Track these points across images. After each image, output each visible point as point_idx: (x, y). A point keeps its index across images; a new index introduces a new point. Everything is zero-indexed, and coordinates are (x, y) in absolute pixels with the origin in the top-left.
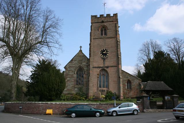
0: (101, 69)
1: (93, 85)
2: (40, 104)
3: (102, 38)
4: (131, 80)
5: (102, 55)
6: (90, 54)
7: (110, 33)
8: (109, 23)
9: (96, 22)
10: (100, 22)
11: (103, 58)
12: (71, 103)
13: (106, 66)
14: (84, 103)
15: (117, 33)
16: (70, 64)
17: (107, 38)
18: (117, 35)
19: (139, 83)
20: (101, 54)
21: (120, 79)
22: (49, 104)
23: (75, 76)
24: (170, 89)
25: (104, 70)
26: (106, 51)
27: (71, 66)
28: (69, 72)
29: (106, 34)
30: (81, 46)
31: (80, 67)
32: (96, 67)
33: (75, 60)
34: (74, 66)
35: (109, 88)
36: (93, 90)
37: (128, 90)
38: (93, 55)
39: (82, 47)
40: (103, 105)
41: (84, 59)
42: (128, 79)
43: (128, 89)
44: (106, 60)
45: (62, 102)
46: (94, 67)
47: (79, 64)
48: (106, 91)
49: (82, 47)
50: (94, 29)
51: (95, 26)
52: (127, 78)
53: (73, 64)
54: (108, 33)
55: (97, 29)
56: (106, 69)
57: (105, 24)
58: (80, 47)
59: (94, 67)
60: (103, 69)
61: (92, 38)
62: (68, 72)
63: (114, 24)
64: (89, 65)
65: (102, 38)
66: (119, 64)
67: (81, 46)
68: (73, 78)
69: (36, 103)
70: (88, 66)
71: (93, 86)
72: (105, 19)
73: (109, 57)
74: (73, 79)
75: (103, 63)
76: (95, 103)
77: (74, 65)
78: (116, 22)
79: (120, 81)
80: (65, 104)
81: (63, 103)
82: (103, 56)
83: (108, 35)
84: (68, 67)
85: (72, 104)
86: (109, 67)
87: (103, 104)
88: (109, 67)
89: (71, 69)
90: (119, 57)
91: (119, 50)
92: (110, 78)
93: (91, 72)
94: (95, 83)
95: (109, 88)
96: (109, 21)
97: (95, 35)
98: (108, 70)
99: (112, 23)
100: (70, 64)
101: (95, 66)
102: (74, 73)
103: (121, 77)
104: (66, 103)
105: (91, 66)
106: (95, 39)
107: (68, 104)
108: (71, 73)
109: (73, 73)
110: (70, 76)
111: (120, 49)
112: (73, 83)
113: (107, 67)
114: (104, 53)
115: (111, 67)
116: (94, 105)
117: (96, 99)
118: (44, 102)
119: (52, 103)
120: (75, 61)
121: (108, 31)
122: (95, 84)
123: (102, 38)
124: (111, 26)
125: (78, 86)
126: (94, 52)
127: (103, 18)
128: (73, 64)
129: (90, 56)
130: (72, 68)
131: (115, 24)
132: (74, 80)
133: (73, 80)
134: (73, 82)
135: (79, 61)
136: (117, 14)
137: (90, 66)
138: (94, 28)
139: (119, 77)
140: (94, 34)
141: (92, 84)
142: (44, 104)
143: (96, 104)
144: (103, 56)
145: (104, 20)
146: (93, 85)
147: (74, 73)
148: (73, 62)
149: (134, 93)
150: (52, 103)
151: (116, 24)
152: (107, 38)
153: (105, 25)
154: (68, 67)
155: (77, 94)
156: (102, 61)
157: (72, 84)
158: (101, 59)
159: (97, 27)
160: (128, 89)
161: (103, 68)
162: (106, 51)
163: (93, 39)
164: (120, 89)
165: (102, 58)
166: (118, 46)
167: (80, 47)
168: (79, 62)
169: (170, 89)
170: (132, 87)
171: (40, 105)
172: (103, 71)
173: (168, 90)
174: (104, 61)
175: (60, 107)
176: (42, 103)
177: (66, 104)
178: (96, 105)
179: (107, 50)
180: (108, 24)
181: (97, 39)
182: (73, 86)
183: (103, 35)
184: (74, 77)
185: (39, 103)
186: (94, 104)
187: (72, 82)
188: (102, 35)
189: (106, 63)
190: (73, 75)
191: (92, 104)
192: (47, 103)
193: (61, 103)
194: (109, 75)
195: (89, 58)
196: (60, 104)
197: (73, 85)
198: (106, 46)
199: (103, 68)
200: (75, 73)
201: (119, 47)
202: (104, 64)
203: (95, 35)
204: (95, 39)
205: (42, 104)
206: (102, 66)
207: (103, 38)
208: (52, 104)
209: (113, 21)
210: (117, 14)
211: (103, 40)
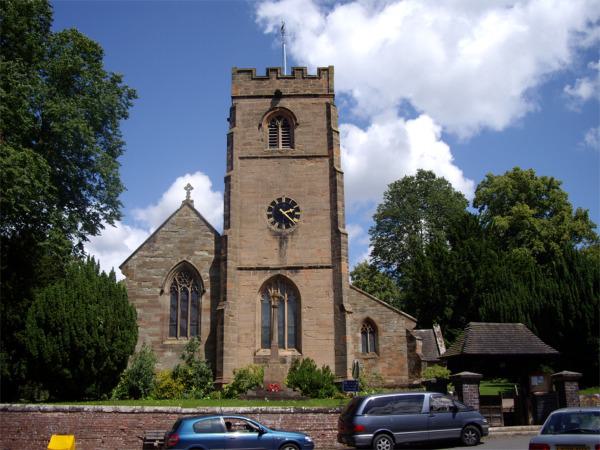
0: (269, 275)
1: (239, 339)
2: (48, 415)
3: (274, 157)
4: (376, 319)
5: (273, 223)
6: (227, 217)
7: (307, 138)
8: (303, 100)
9: (252, 94)
10: (266, 93)
11: (280, 234)
12: (255, 408)
13: (290, 263)
14: (232, 409)
15: (332, 138)
16: (146, 253)
17: (294, 157)
18: (332, 148)
19: (407, 331)
20: (269, 216)
21: (344, 316)
22: (87, 412)
23: (166, 300)
24: (549, 350)
25: (281, 286)
26: (291, 210)
27: (147, 260)
28: (140, 284)
29: (289, 141)
30: (189, 185)
31: (185, 266)
32: (251, 269)
33: (166, 240)
34: (161, 263)
35: (300, 351)
36: (241, 355)
37: (366, 359)
38: (241, 221)
39: (192, 188)
40: (310, 415)
41: (200, 234)
42: (365, 315)
43: (368, 356)
44: (290, 243)
45: (143, 405)
46: (240, 269)
47: (182, 253)
48: (289, 360)
49: (192, 188)
50: (243, 121)
51: (248, 109)
52: (363, 311)
53: (156, 253)
54: (298, 138)
55: (256, 123)
56: (288, 274)
57: (285, 103)
58: (186, 188)
59: (240, 269)
60: (279, 276)
61: (237, 153)
62: (136, 284)
63: (321, 104)
64: (225, 260)
65: (275, 155)
66: (340, 259)
67: (189, 185)
68: (159, 311)
69: (29, 411)
70: (219, 264)
71: (238, 342)
72: (286, 86)
73: (299, 231)
74: (156, 315)
75: (276, 254)
76: (280, 409)
77: (161, 259)
78: (328, 100)
79: (344, 321)
80: (156, 412)
81: (147, 409)
82: (277, 224)
83: (296, 145)
84: (139, 266)
85: (184, 410)
86: (302, 268)
87: (308, 412)
88: (302, 268)
89: (149, 274)
90: (341, 230)
91: (339, 204)
92: (303, 310)
93: (230, 287)
94: (248, 331)
95: (303, 349)
96: (302, 92)
97: (250, 144)
98: (299, 279)
99: (314, 100)
100: (146, 253)
101: (245, 264)
102: (162, 292)
103: (347, 309)
104: (160, 408)
105: (229, 263)
106: (248, 158)
107: (167, 413)
108: (146, 291)
109: (159, 290)
110: (146, 301)
111: (343, 200)
112: (157, 329)
113: (296, 269)
114: (282, 214)
115: (310, 268)
116: (275, 416)
117: (261, 391)
118: (67, 406)
119: (100, 407)
120: (164, 243)
121: (297, 131)
122: (247, 334)
123: (274, 157)
124: (307, 112)
125: (176, 342)
126: (241, 207)
127: (278, 81)
128: (156, 253)
129: (227, 225)
130: (152, 271)
131: (325, 107)
132: (162, 320)
133: (158, 319)
134: (155, 324)
135: (181, 242)
136: (332, 68)
137: (226, 264)
138: (243, 115)
139: (342, 309)
140: (244, 138)
141: (236, 335)
142: (65, 411)
143: (282, 413)
144: (277, 224)
145: (282, 90)
146: (239, 339)
147: (162, 292)
148: (156, 245)
149: (389, 369)
150: (100, 407)
151: (328, 106)
152: (294, 157)
153: (288, 106)
154: (136, 263)
155: (174, 376)
156: (276, 245)
157: (151, 335)
158: (269, 238)
159: (258, 114)
160: (368, 356)
161: (279, 272)
162: (291, 210)
163: (241, 158)
164: (345, 355)
165: (276, 235)
166: (338, 188)
167: (186, 188)
168: (179, 248)
169: (549, 350)
170: (382, 346)
171: (47, 418)
172: (276, 282)
173: (543, 352)
174: (281, 244)
175: (134, 426)
176: (57, 411)
177: (161, 412)
178: (282, 416)
179: (298, 210)
180: (299, 106)
181: (255, 161)
182: (157, 343)
183: (277, 146)
184: (160, 306)
185: (45, 411)
186: (273, 413)
187: (152, 324)
188: (273, 143)
189: (288, 251)
190: (157, 296)
191: (266, 412)
192: (79, 410)
193: (139, 407)
194: (303, 298)
195: (217, 222)
196: (133, 412)
197: (156, 339)
198: (287, 189)
199: (279, 272)
200: (167, 289)
201: (339, 194)
202: (282, 255)
203: (250, 144)
204: (248, 158)
205: (56, 415)
206: (273, 262)
207: (279, 157)
208: (101, 411)
209: (316, 96)
210: (332, 68)
211: (277, 165)
